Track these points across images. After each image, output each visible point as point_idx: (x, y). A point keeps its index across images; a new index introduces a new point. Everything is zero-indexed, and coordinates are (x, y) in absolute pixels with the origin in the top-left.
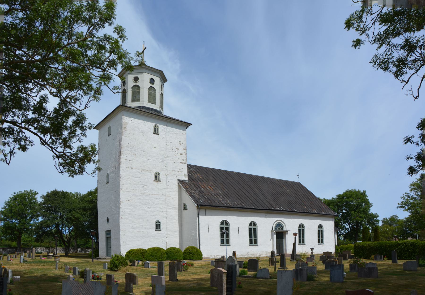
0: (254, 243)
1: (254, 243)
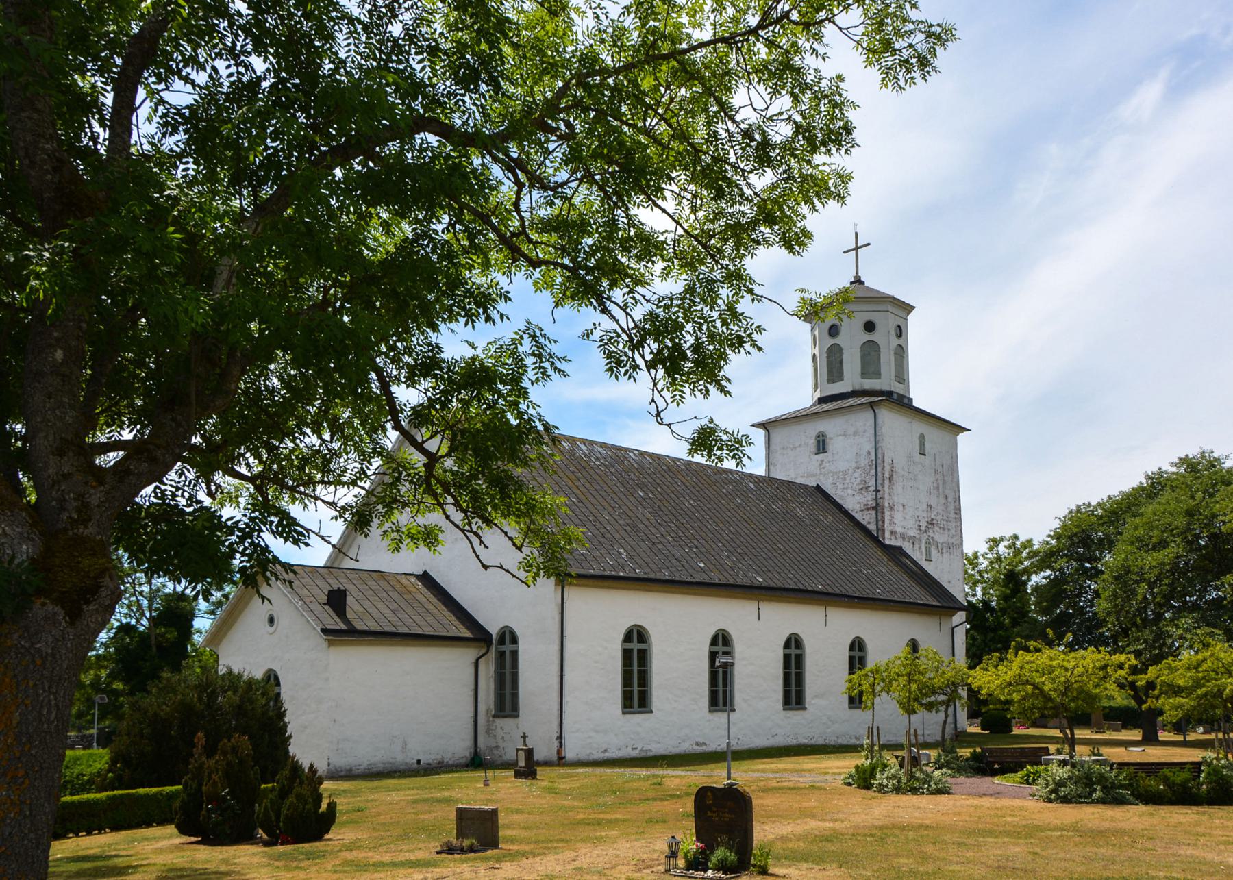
0: (640, 706)
1: (640, 706)
